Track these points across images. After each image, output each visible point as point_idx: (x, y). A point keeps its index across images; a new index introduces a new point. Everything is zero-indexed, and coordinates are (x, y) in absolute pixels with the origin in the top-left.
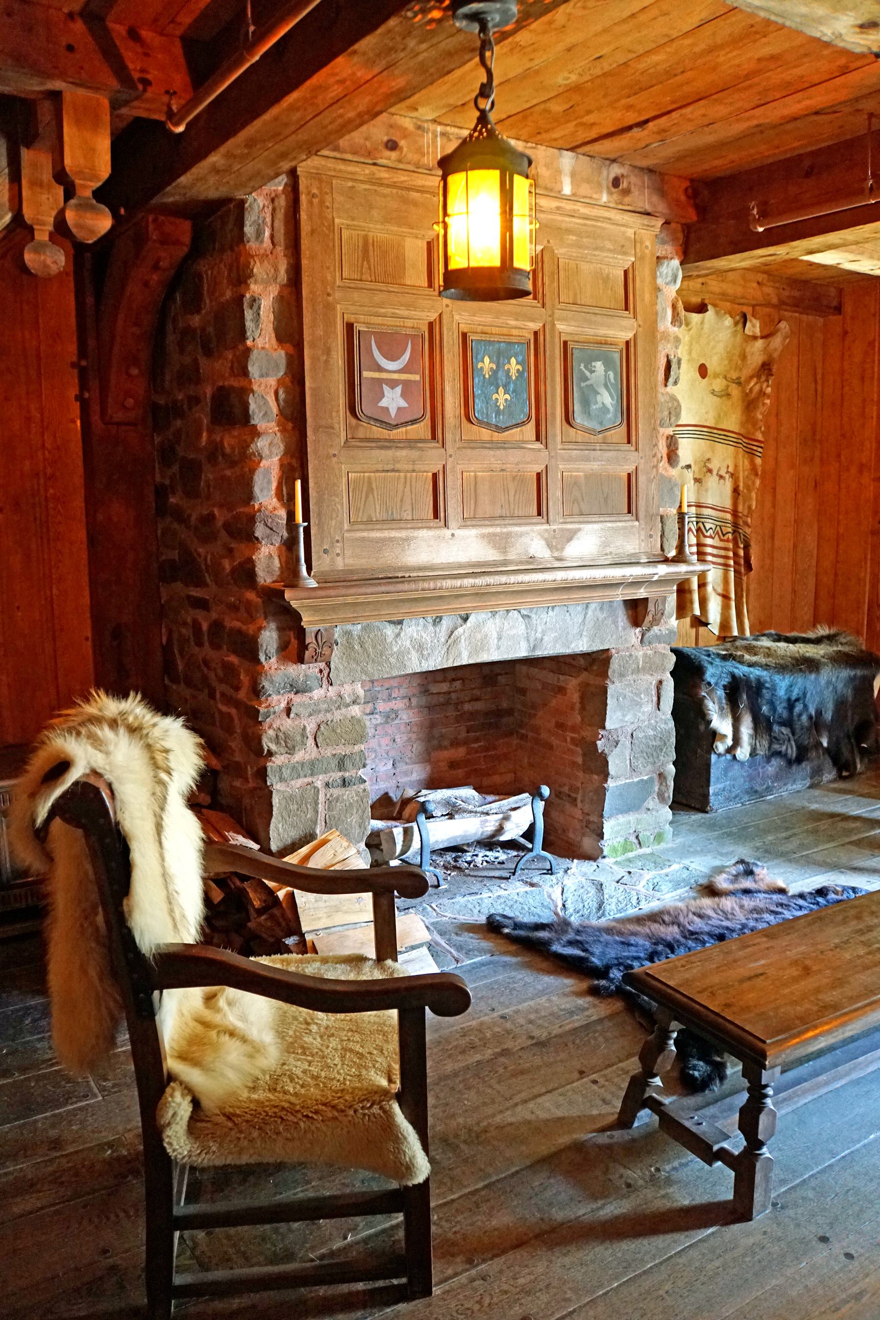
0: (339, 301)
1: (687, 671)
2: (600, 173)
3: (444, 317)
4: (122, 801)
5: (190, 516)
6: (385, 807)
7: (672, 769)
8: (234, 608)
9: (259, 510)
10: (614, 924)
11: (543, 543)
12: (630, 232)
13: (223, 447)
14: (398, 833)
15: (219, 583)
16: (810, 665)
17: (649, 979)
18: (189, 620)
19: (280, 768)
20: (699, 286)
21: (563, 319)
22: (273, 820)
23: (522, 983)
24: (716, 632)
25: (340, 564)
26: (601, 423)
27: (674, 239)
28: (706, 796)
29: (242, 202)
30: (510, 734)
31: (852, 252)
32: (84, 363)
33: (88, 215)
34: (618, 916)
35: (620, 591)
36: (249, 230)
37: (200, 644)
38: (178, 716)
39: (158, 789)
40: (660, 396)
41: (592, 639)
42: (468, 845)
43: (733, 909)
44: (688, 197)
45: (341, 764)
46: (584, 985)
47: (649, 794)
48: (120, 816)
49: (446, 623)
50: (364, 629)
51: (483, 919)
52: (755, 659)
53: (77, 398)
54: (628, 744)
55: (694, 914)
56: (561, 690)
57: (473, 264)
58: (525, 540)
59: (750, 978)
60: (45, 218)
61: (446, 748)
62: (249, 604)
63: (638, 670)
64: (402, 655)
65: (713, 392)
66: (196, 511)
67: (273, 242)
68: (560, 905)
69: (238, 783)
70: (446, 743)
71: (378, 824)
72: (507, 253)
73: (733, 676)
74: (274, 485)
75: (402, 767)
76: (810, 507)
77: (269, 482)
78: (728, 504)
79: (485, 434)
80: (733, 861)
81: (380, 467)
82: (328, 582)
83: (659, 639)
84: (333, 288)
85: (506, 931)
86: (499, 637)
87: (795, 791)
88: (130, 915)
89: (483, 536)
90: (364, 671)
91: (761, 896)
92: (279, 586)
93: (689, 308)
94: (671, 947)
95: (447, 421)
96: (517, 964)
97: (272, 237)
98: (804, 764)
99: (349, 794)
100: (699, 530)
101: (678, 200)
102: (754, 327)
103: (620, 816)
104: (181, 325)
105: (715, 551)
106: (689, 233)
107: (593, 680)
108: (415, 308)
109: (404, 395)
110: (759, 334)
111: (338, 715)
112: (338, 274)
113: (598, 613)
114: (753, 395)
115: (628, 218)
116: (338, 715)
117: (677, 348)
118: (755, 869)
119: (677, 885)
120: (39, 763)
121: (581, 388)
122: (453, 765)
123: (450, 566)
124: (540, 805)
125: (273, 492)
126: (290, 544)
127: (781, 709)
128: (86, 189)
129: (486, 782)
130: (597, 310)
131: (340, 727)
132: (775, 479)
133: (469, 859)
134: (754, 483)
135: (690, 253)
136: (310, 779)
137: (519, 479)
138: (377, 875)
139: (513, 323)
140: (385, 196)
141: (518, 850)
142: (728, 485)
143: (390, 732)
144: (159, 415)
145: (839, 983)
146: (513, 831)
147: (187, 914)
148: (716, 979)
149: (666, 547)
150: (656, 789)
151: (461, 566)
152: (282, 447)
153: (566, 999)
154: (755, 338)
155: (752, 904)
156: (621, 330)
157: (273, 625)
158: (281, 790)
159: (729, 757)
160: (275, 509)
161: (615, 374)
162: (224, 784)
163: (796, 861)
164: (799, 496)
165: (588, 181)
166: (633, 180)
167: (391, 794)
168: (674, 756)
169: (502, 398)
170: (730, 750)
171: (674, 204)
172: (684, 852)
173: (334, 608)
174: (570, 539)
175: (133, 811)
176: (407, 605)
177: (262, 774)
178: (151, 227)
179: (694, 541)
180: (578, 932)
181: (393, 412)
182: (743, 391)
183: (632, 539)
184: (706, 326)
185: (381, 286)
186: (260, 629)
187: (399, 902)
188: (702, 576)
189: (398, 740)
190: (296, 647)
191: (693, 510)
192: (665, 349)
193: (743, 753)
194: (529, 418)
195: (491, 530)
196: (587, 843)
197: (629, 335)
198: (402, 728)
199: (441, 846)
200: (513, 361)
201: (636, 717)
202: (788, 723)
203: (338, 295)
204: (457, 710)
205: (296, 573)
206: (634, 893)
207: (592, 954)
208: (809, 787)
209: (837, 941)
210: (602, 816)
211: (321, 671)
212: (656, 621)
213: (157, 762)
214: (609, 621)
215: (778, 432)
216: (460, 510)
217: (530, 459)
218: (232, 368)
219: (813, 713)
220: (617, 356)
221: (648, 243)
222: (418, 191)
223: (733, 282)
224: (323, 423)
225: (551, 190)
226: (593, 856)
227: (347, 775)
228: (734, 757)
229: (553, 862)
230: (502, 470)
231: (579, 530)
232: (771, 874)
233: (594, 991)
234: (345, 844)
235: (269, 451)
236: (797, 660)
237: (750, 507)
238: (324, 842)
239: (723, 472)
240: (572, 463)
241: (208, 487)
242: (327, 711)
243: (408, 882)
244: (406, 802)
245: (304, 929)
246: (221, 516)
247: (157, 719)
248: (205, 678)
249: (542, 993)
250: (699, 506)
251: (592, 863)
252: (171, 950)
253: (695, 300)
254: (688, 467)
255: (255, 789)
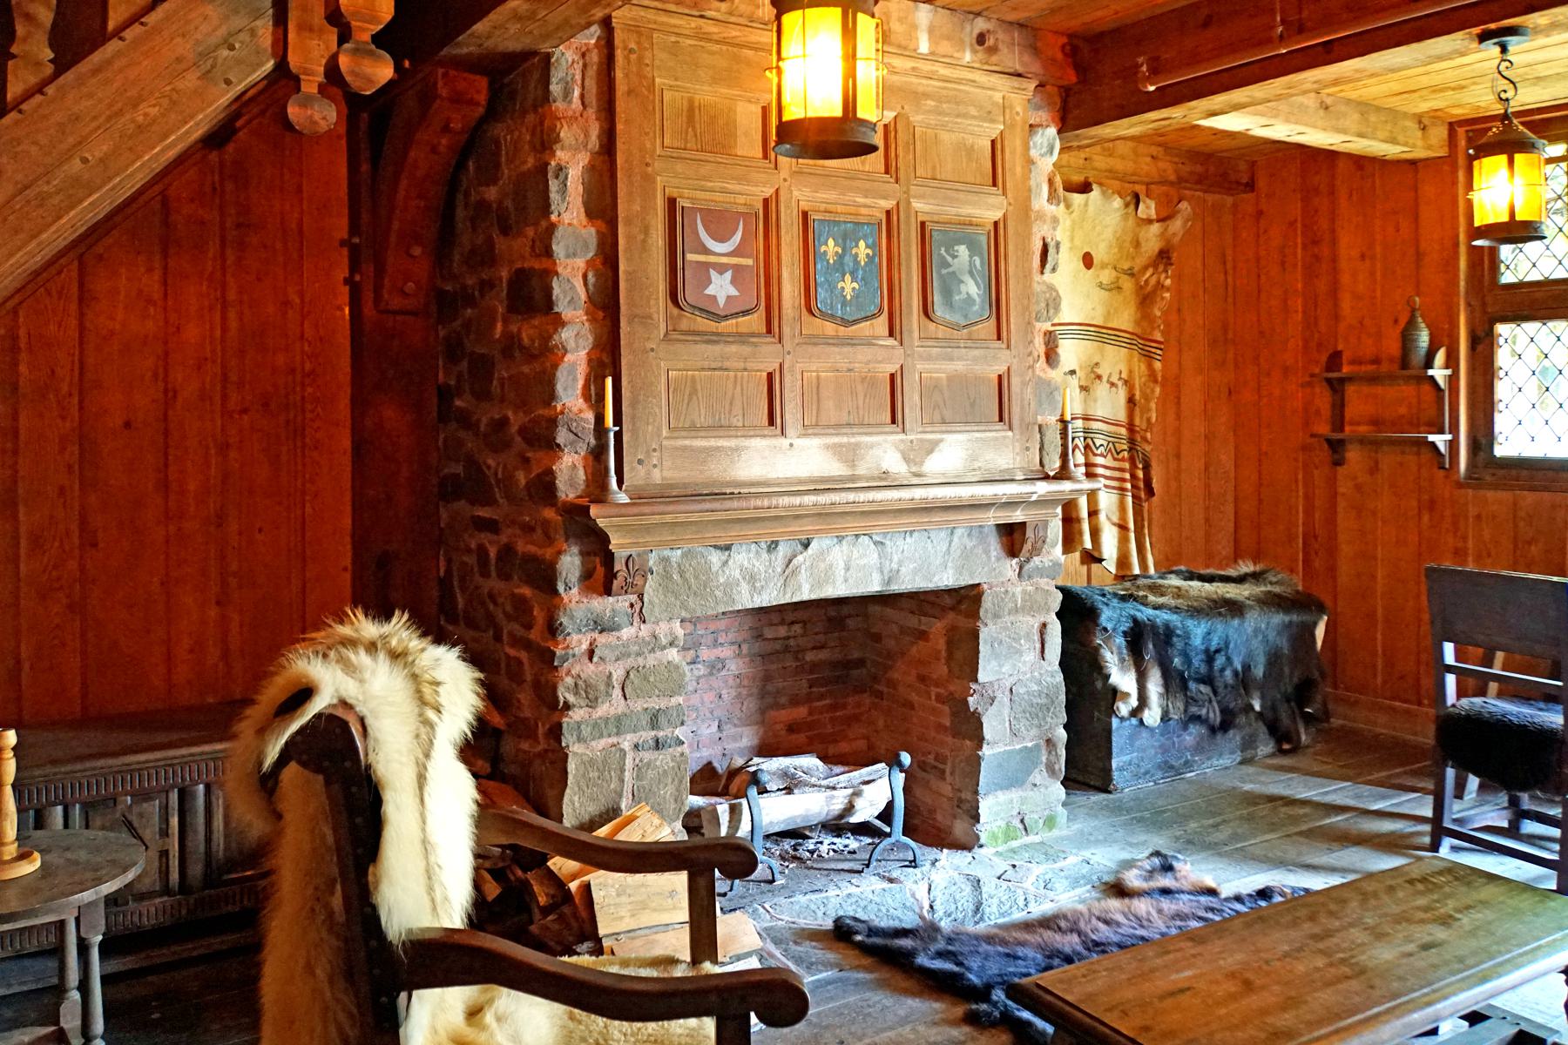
0: (659, 174)
1: (1077, 613)
2: (963, 29)
3: (782, 193)
4: (376, 740)
5: (479, 420)
6: (708, 780)
7: (1062, 735)
8: (529, 529)
9: (562, 413)
10: (996, 931)
11: (898, 456)
12: (998, 97)
13: (520, 339)
14: (723, 809)
15: (510, 498)
16: (1233, 608)
17: (1041, 993)
18: (473, 546)
19: (579, 724)
20: (1082, 161)
21: (922, 196)
22: (568, 791)
23: (879, 1006)
24: (1113, 570)
25: (657, 476)
26: (966, 317)
27: (1050, 104)
28: (1107, 773)
29: (548, 56)
30: (860, 690)
31: (1263, 115)
32: (356, 240)
33: (366, 62)
34: (1001, 921)
35: (991, 513)
36: (555, 88)
37: (485, 574)
38: (454, 645)
39: (423, 730)
40: (1035, 285)
41: (959, 570)
42: (810, 828)
43: (1149, 913)
44: (1065, 55)
45: (654, 723)
46: (959, 1011)
47: (1035, 764)
48: (371, 757)
49: (783, 550)
50: (684, 555)
51: (828, 924)
52: (1161, 600)
53: (346, 281)
54: (1006, 700)
55: (1099, 919)
56: (923, 635)
57: (811, 114)
58: (876, 452)
59: (1172, 994)
60: (315, 67)
61: (783, 707)
62: (546, 524)
63: (1016, 610)
64: (730, 586)
65: (1101, 285)
66: (486, 415)
67: (583, 104)
68: (927, 907)
69: (525, 746)
70: (783, 700)
71: (698, 801)
72: (850, 104)
73: (1135, 620)
74: (581, 383)
75: (729, 730)
76: (1223, 419)
77: (575, 380)
78: (1122, 416)
79: (830, 328)
80: (1147, 853)
81: (706, 364)
82: (642, 497)
83: (1041, 572)
84: (652, 156)
85: (859, 938)
86: (846, 569)
87: (1221, 766)
88: (376, 888)
89: (827, 447)
90: (684, 606)
91: (1185, 897)
92: (584, 501)
93: (1070, 188)
94: (1068, 960)
95: (784, 312)
96: (871, 981)
97: (582, 96)
98: (1231, 732)
99: (663, 759)
100: (1087, 447)
101: (1054, 60)
102: (1148, 208)
103: (999, 793)
104: (473, 198)
105: (1108, 473)
106: (1067, 96)
107: (962, 622)
108: (749, 182)
109: (734, 282)
110: (1154, 216)
111: (651, 660)
112: (658, 141)
113: (966, 540)
114: (1149, 288)
115: (995, 80)
116: (651, 660)
117: (1054, 229)
118: (1175, 864)
119: (1075, 882)
120: (274, 692)
121: (941, 276)
122: (792, 728)
123: (788, 481)
124: (900, 778)
125: (579, 392)
126: (598, 453)
127: (1198, 662)
128: (364, 33)
129: (832, 750)
130: (958, 186)
131: (654, 688)
132: (1178, 386)
133: (812, 847)
134: (1153, 391)
135: (1068, 121)
136: (614, 740)
137: (870, 382)
138: (695, 848)
139: (861, 200)
140: (712, 53)
141: (873, 836)
142: (1121, 395)
143: (715, 685)
144: (446, 304)
145: (1290, 1003)
146: (866, 811)
147: (451, 895)
148: (1129, 994)
149: (1046, 461)
150: (1044, 759)
151: (801, 482)
152: (591, 339)
153: (934, 1030)
154: (1150, 221)
155: (1174, 907)
156: (989, 209)
157: (575, 550)
158: (579, 752)
159: (1134, 721)
160: (581, 411)
161: (982, 263)
162: (508, 746)
163: (1228, 855)
164: (1209, 406)
165: (948, 38)
166: (1000, 37)
167: (716, 764)
168: (1064, 718)
169: (849, 286)
170: (1135, 713)
171: (1049, 63)
172: (1084, 840)
173: (648, 529)
174: (930, 451)
175: (390, 752)
176: (738, 526)
177: (556, 732)
178: (440, 84)
179: (1081, 459)
180: (950, 940)
181: (721, 301)
182: (1137, 283)
183: (1004, 452)
184: (1091, 208)
185: (709, 156)
186: (560, 553)
187: (721, 885)
188: (1092, 495)
189: (725, 696)
190: (603, 574)
191: (1079, 423)
192: (1040, 231)
193: (1152, 716)
194: (881, 310)
195: (836, 440)
196: (959, 828)
197: (997, 215)
198: (731, 682)
199: (777, 829)
200: (862, 244)
201: (1017, 670)
202: (1208, 680)
203: (657, 165)
204: (797, 659)
205: (604, 486)
206: (1020, 892)
207: (969, 969)
208: (1241, 763)
209: (1286, 948)
210: (976, 793)
211: (632, 606)
212: (1036, 551)
213: (424, 698)
214: (979, 550)
215: (1181, 333)
216: (800, 416)
217: (883, 357)
218: (533, 247)
219: (1239, 668)
220: (984, 239)
221: (1019, 109)
222: (751, 48)
223: (1123, 157)
224: (638, 311)
225: (905, 48)
226: (967, 844)
227: (661, 734)
228: (1141, 721)
229: (918, 852)
230: (850, 370)
231: (941, 440)
232: (1195, 870)
233: (972, 1019)
234: (657, 821)
235: (576, 343)
236: (1214, 601)
237: (1149, 420)
238: (630, 820)
239: (1114, 379)
240: (930, 363)
241: (502, 386)
242: (639, 654)
243: (733, 857)
244: (733, 773)
245: (602, 932)
246: (516, 420)
247: (424, 643)
248: (490, 618)
249: (904, 1021)
250: (1086, 418)
251: (965, 853)
252: (427, 936)
253: (1077, 178)
254: (1073, 372)
255: (546, 751)
